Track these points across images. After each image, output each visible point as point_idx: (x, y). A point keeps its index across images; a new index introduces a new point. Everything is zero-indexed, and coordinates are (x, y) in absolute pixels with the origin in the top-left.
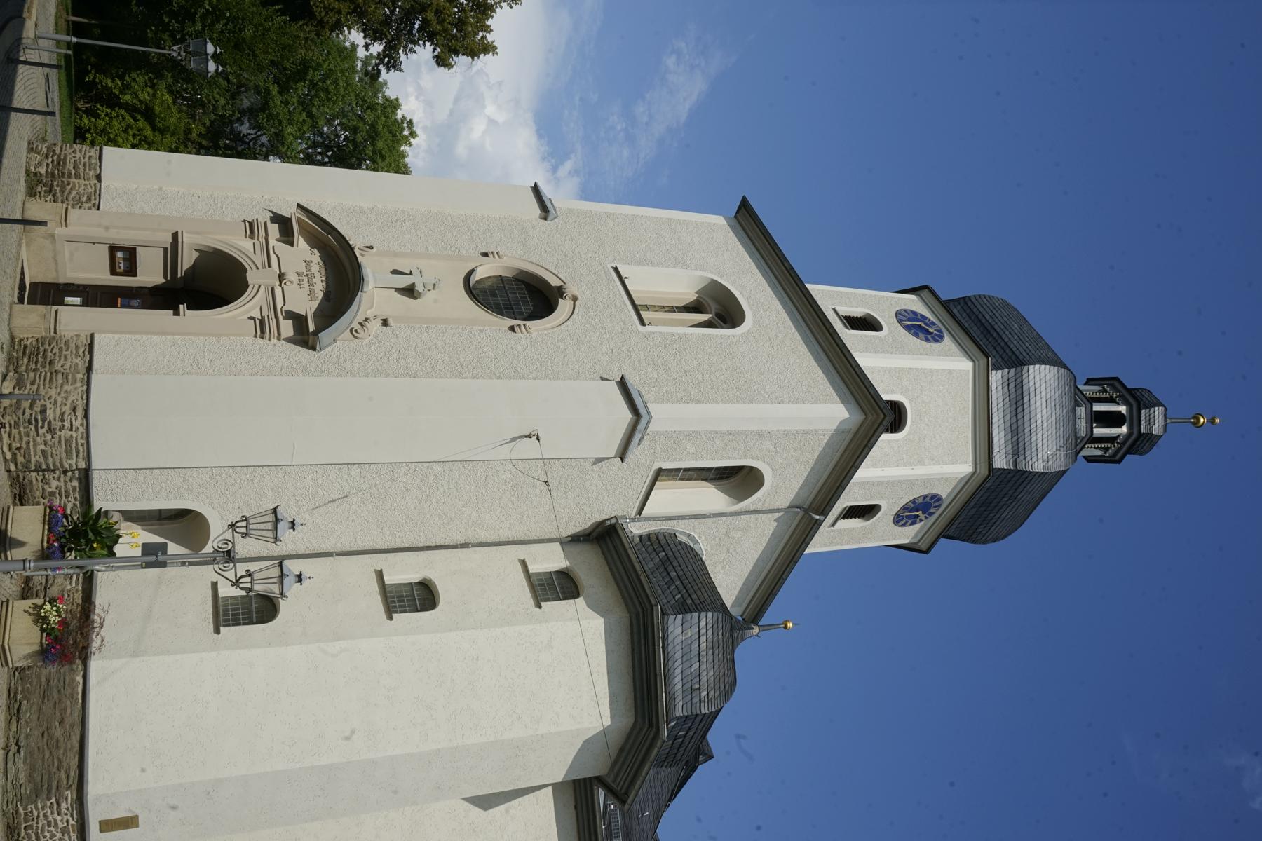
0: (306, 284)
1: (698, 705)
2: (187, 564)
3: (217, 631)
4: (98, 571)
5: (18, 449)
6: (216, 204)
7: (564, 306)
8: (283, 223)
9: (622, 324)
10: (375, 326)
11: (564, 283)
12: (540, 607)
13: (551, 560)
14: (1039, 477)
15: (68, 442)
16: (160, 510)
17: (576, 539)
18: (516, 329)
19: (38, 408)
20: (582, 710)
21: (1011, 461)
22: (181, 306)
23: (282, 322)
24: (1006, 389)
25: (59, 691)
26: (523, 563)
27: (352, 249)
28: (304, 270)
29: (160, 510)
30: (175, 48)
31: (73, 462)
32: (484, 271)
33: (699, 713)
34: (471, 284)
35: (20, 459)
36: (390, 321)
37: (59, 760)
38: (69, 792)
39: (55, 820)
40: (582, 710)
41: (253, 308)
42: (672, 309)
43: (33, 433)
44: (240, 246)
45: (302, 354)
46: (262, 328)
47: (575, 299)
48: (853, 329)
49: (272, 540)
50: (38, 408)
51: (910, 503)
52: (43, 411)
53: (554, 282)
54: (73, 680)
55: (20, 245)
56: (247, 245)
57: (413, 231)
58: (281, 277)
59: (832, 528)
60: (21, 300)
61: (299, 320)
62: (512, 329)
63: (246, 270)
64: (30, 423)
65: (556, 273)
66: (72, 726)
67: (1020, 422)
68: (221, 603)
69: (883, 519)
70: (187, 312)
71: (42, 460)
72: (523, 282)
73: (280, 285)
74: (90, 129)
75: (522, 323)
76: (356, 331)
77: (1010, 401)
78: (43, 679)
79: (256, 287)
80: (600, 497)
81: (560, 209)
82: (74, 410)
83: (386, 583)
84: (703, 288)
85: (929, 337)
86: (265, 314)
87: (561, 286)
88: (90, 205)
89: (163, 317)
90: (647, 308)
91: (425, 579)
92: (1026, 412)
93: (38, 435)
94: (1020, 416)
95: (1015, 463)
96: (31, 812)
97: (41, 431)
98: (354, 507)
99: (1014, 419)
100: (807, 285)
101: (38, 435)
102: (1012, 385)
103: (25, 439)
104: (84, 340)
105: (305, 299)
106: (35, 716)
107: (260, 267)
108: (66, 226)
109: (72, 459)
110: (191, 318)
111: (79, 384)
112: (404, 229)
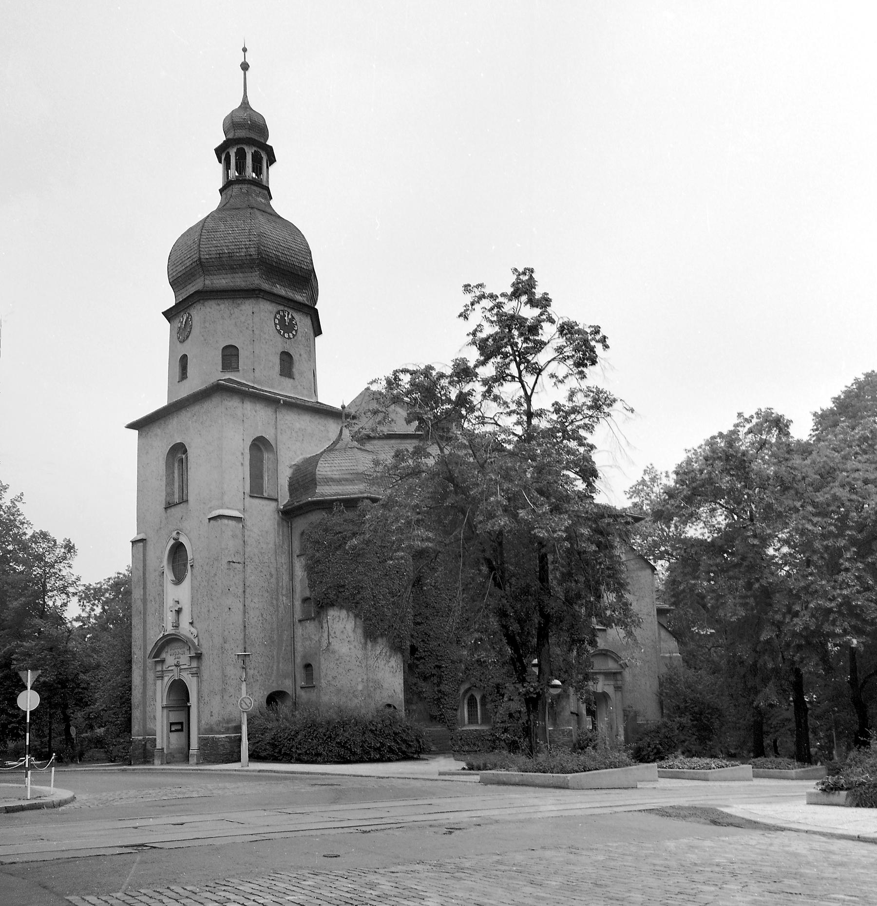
7: (183, 539)
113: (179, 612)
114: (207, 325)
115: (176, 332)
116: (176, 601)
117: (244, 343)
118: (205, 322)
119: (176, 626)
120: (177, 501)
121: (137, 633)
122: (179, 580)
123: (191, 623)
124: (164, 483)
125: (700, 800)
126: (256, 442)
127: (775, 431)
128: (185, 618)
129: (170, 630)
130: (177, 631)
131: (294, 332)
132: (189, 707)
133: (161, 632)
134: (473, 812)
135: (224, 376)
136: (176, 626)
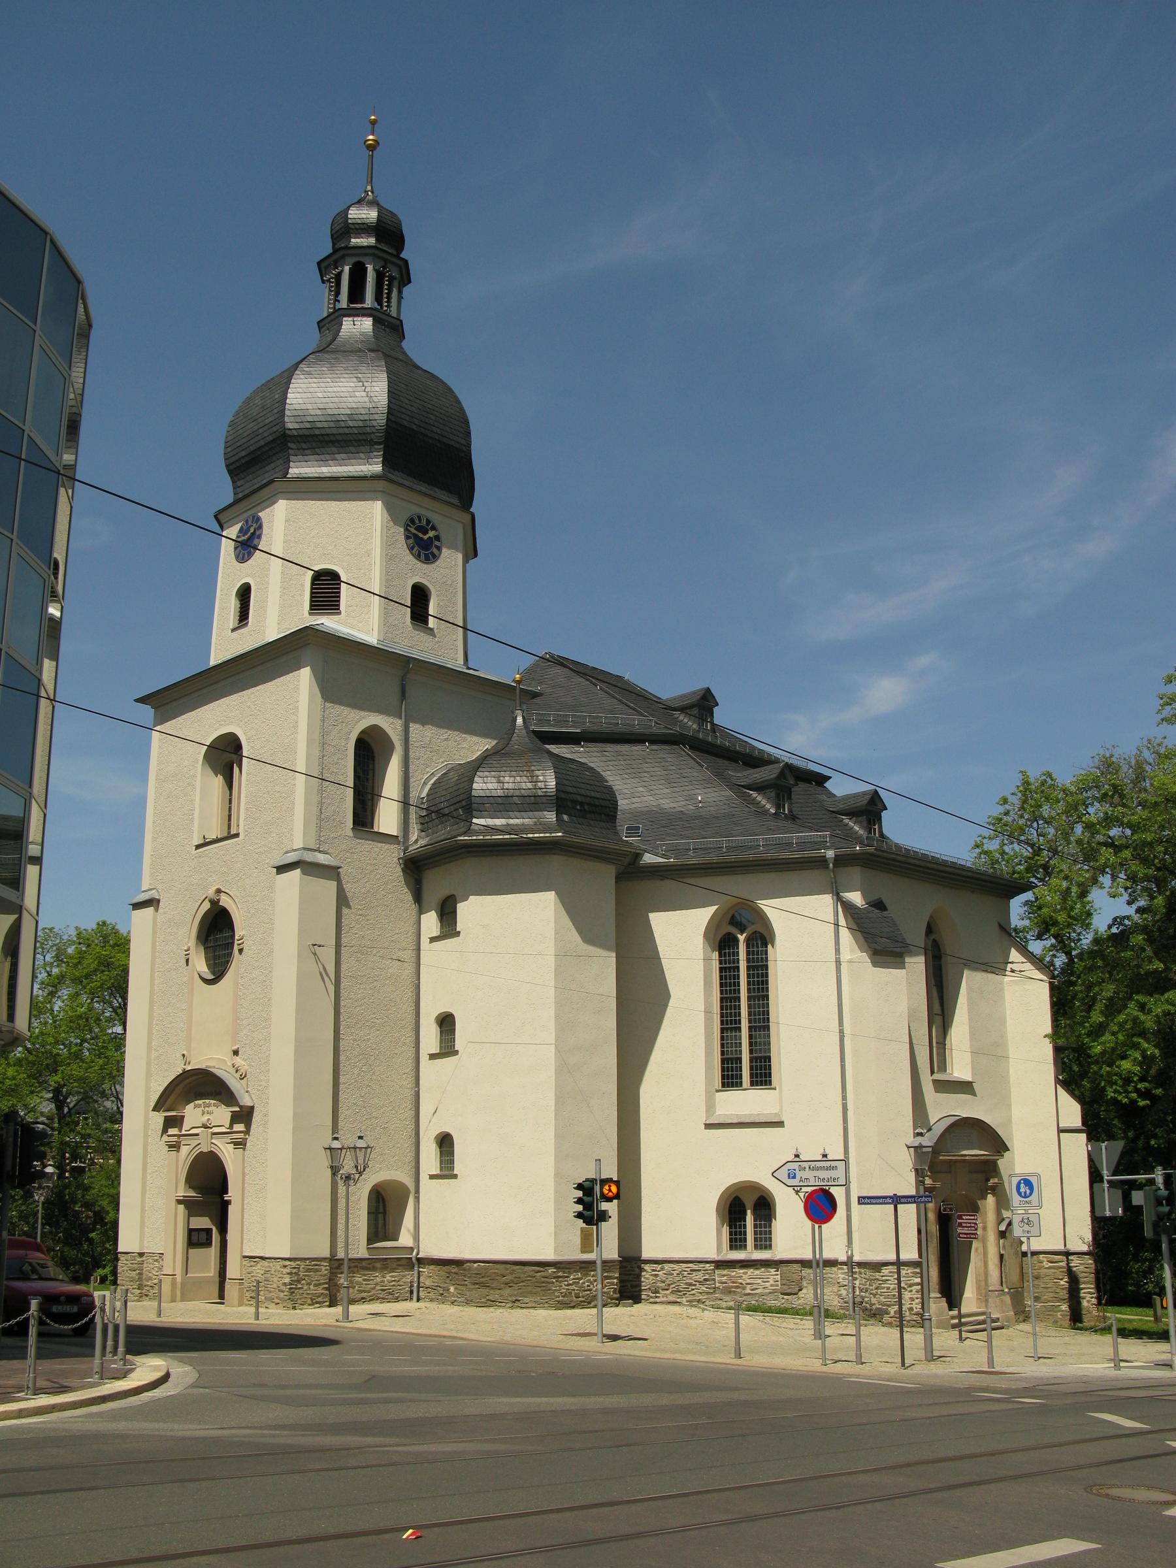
0: (210, 1109)
1: (548, 798)
2: (63, 1299)
3: (455, 1176)
4: (418, 1254)
5: (312, 1299)
6: (157, 1171)
7: (225, 901)
8: (169, 1123)
9: (237, 853)
10: (238, 1060)
11: (206, 898)
12: (459, 932)
13: (430, 922)
14: (393, 415)
15: (308, 1270)
16: (368, 1213)
17: (418, 898)
18: (241, 947)
19: (283, 1288)
20: (540, 900)
21: (376, 447)
22: (225, 1198)
23: (235, 1130)
24: (307, 452)
25: (483, 1277)
27: (185, 1072)
28: (200, 1109)
29: (369, 1213)
30: (37, 1198)
31: (324, 1268)
32: (201, 965)
33: (554, 801)
34: (212, 977)
35: (320, 1299)
36: (235, 1048)
37: (527, 1277)
38: (550, 1271)
39: (574, 1279)
40: (540, 900)
41: (226, 1148)
42: (231, 795)
43: (301, 1291)
44: (186, 1153)
45: (257, 1117)
46: (240, 1144)
47: (219, 891)
48: (247, 618)
49: (369, 1150)
50: (283, 1288)
51: (414, 551)
52: (285, 1284)
53: (207, 906)
54: (476, 1268)
55: (1107, 1496)
56: (184, 1150)
57: (170, 1019)
58: (205, 1126)
59: (436, 631)
60: (223, 1303)
61: (235, 1118)
62: (241, 951)
63: (201, 1152)
64: (293, 1292)
65: (200, 901)
66: (507, 1269)
67: (339, 438)
68: (444, 1173)
69: (433, 575)
70: (229, 1195)
71: (322, 1287)
72: (208, 936)
73: (211, 1128)
74: (106, 1224)
75: (236, 942)
76: (241, 1075)
77: (319, 448)
78: (473, 1287)
79: (212, 1145)
80: (378, 876)
81: (150, 884)
82: (285, 1266)
83: (438, 1052)
84: (213, 770)
85: (258, 533)
86: (230, 1141)
87: (210, 901)
88: (160, 1260)
89: (233, 1212)
90: (229, 832)
91: (437, 1022)
92: (329, 431)
93: (302, 1288)
94: (332, 438)
95: (379, 444)
96: (562, 1293)
97: (299, 1286)
98: (374, 1077)
99: (337, 444)
100: (213, 663)
101: (302, 1288)
102: (304, 446)
103: (305, 1295)
104: (246, 1262)
105: (221, 1114)
106: (498, 1292)
107: (199, 1142)
108: (175, 1275)
109: (593, 1252)
110: (233, 1194)
111: (271, 1265)
112: (169, 1026)
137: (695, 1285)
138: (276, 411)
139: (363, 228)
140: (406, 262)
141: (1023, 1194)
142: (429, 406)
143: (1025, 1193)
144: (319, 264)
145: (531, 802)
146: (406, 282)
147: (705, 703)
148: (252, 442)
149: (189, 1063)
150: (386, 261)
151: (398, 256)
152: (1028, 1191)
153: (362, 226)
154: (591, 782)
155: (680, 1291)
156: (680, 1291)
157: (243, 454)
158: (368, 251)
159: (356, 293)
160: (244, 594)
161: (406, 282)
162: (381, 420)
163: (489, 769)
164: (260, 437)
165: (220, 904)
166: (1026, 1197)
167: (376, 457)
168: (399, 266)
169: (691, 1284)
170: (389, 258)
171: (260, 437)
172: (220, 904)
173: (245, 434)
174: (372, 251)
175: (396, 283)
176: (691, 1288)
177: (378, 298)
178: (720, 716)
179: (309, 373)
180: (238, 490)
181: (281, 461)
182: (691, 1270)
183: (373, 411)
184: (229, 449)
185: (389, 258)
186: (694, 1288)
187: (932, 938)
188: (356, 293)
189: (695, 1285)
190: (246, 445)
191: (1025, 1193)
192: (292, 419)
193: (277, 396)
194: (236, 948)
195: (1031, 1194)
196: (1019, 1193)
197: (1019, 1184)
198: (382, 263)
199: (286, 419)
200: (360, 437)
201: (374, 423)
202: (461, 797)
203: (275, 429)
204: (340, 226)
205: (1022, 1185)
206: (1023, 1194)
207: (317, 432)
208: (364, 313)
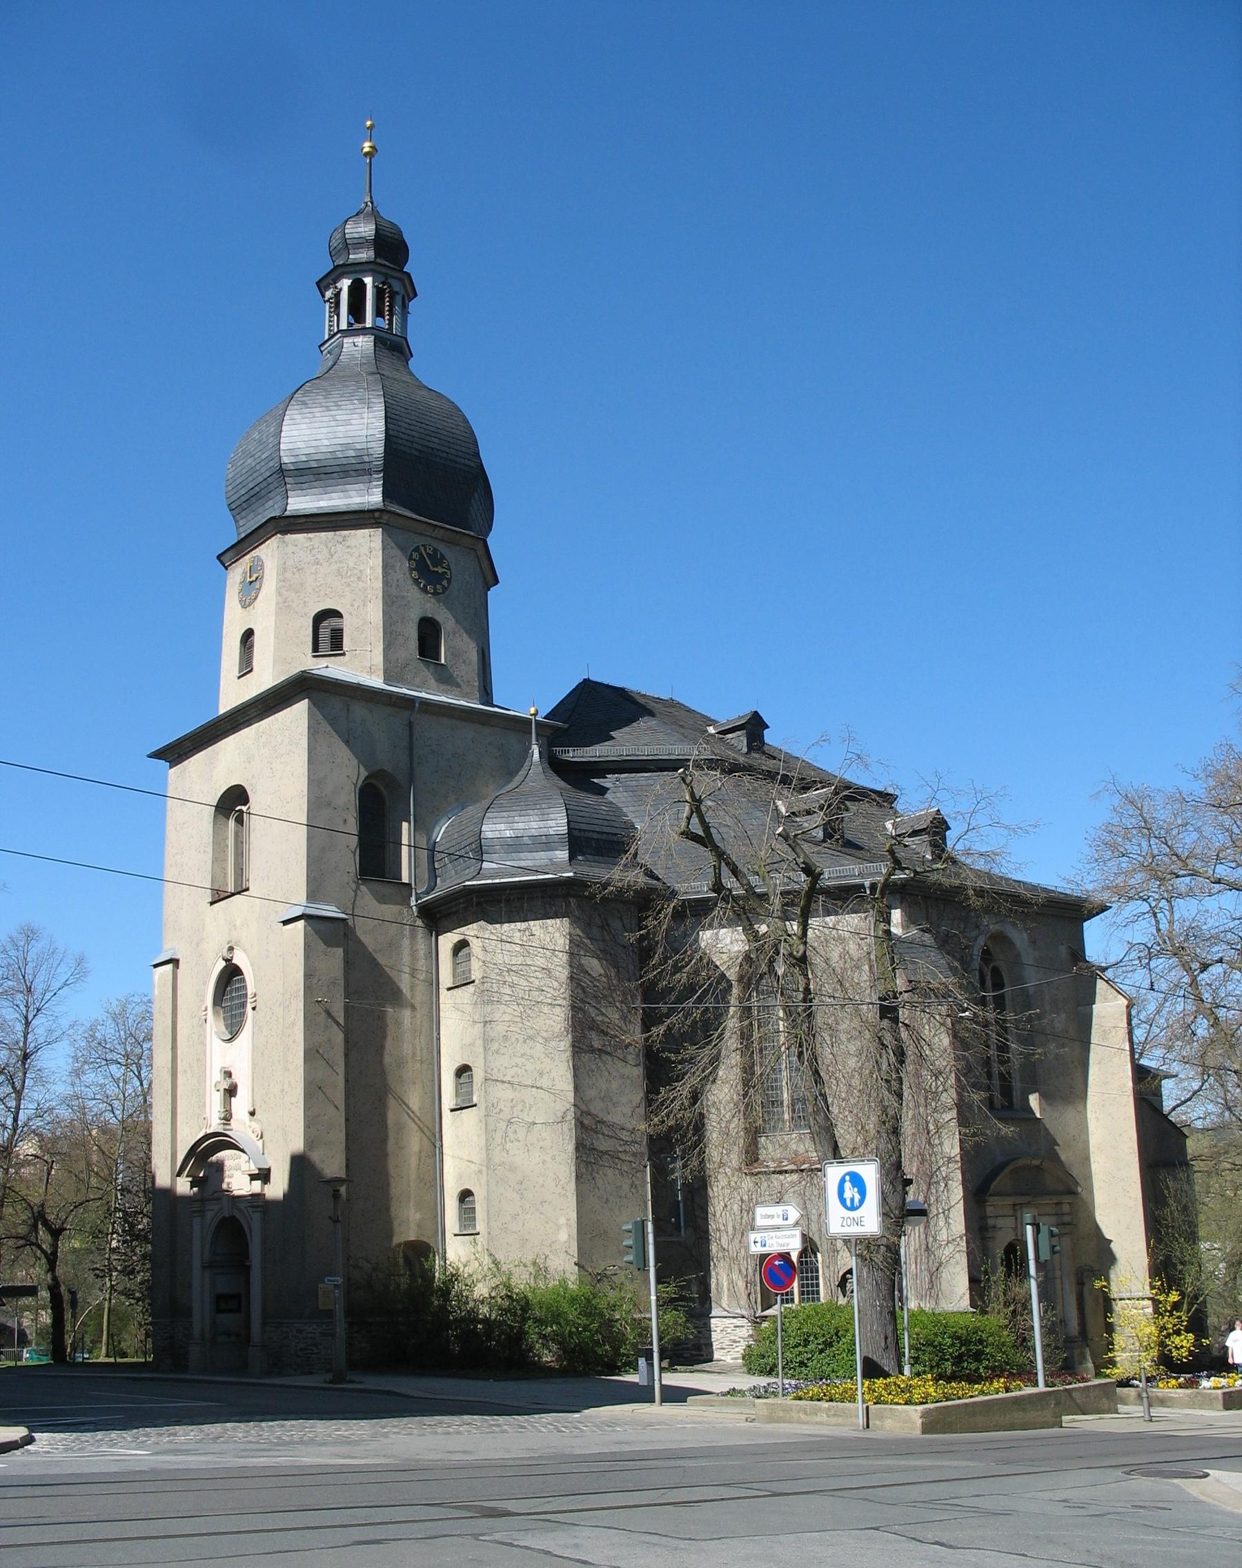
7: (239, 959)
26: (449, 989)
100: (223, 709)
113: (231, 1092)
114: (289, 575)
115: (238, 591)
116: (225, 1072)
117: (352, 605)
118: (285, 570)
119: (227, 1118)
120: (231, 889)
121: (160, 1132)
122: (234, 1030)
123: (252, 1114)
124: (209, 857)
125: (261, 519)
126: (373, 781)
127: (1226, 1326)
128: (240, 1105)
129: (215, 1125)
130: (228, 1127)
131: (445, 583)
132: (249, 1268)
133: (201, 1130)
134: (357, 1538)
135: (317, 664)
136: (227, 1118)
137: (739, 1342)
138: (271, 445)
139: (360, 243)
140: (408, 274)
141: (848, 1203)
142: (433, 429)
143: (852, 1200)
144: (318, 283)
145: (544, 843)
146: (412, 296)
147: (754, 726)
148: (250, 479)
149: (210, 1126)
150: (386, 276)
151: (401, 271)
152: (857, 1197)
153: (360, 241)
154: (608, 818)
155: (724, 1349)
156: (724, 1349)
157: (243, 491)
158: (366, 267)
159: (357, 310)
160: (248, 635)
161: (412, 296)
162: (378, 449)
163: (499, 810)
164: (257, 474)
165: (233, 962)
166: (853, 1208)
167: (376, 487)
168: (402, 280)
169: (735, 1341)
170: (389, 272)
171: (257, 474)
172: (233, 962)
173: (244, 471)
174: (372, 267)
175: (398, 299)
176: (735, 1344)
177: (379, 313)
178: (769, 737)
179: (304, 403)
180: (241, 530)
181: (279, 497)
182: (735, 1327)
183: (369, 439)
184: (230, 488)
185: (389, 272)
186: (738, 1344)
187: (992, 965)
188: (357, 310)
189: (739, 1342)
190: (245, 483)
191: (852, 1200)
192: (288, 453)
193: (272, 429)
194: (249, 1007)
195: (862, 1202)
196: (842, 1201)
197: (843, 1181)
198: (382, 279)
199: (282, 453)
200: (358, 467)
201: (371, 451)
202: (471, 840)
203: (271, 464)
204: (338, 242)
205: (848, 1185)
206: (848, 1203)
207: (314, 465)
208: (364, 331)
